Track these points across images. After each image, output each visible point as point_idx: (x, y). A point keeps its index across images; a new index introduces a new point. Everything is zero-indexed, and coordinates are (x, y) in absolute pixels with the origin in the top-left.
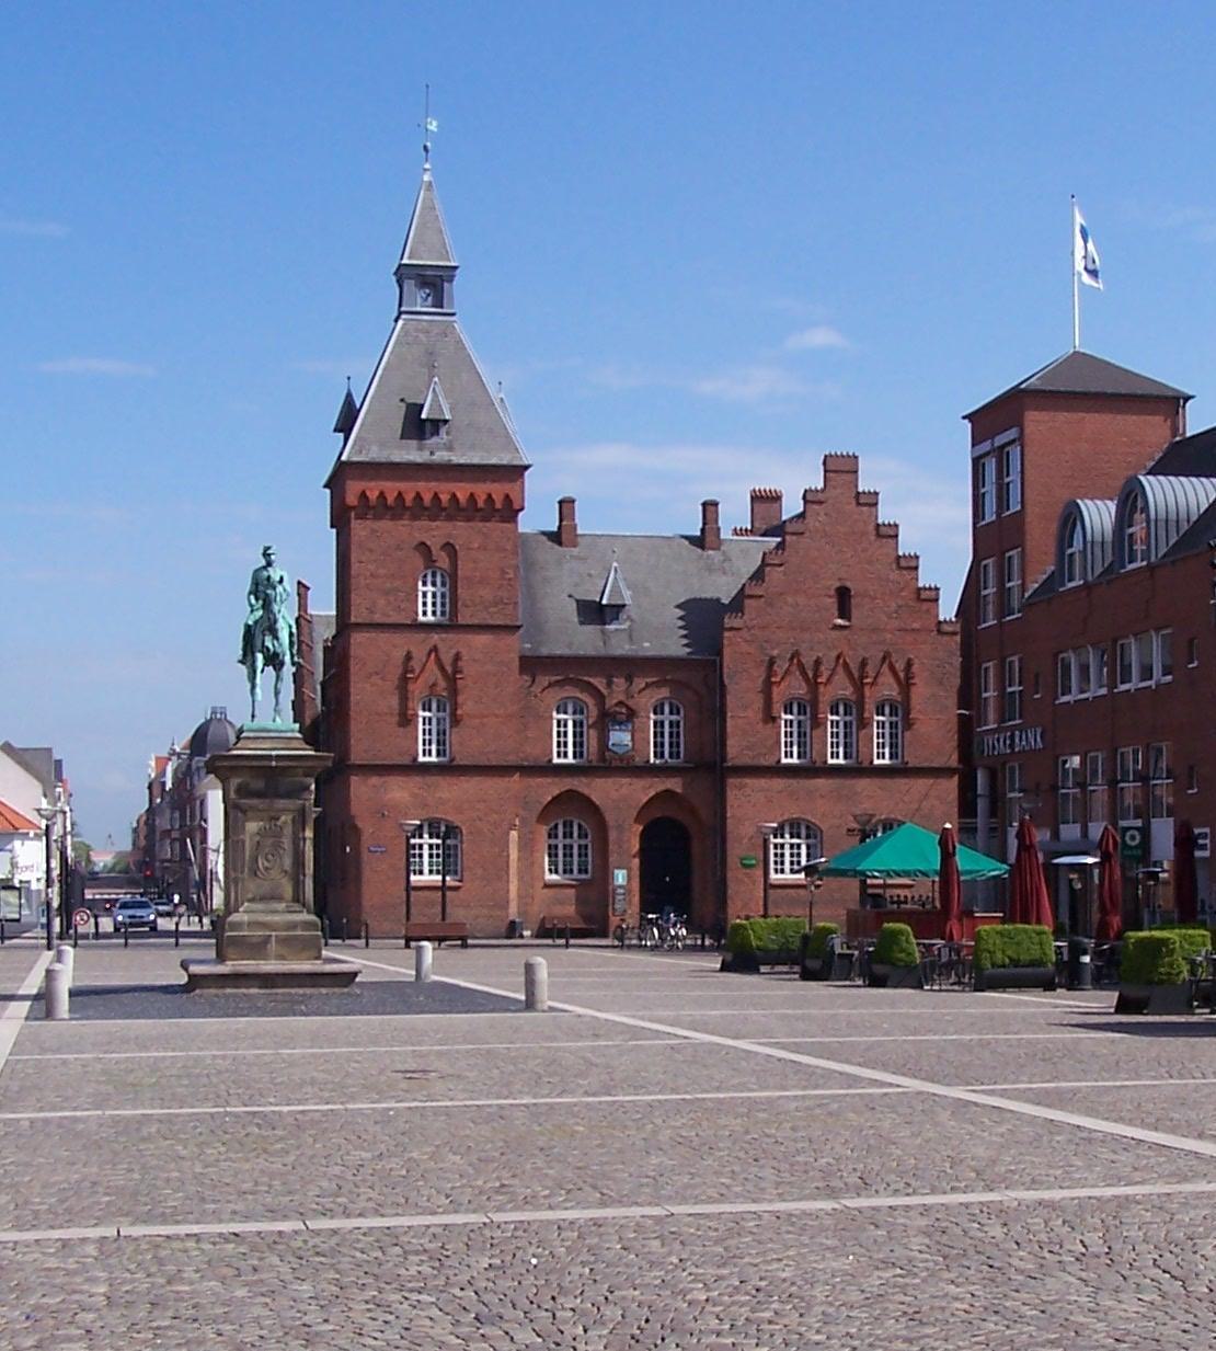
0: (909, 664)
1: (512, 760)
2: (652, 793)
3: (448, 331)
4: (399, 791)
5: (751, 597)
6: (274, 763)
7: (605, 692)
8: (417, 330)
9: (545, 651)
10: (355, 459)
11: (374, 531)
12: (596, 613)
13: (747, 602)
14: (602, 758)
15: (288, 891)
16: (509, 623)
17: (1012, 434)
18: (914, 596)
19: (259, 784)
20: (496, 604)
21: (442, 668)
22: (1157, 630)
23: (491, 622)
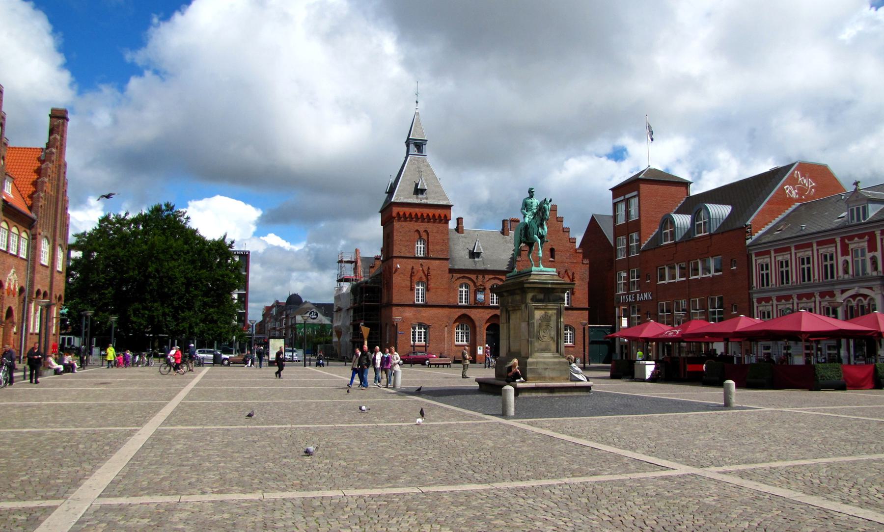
0: (573, 274)
1: (446, 303)
2: (490, 315)
3: (424, 161)
4: (409, 313)
5: (523, 251)
6: (550, 286)
7: (476, 281)
8: (414, 160)
9: (456, 267)
10: (396, 201)
11: (401, 225)
12: (473, 255)
13: (522, 252)
14: (475, 303)
15: (553, 347)
16: (445, 257)
17: (635, 193)
18: (574, 251)
19: (541, 296)
20: (441, 251)
21: (424, 272)
22: (712, 257)
23: (439, 257)
